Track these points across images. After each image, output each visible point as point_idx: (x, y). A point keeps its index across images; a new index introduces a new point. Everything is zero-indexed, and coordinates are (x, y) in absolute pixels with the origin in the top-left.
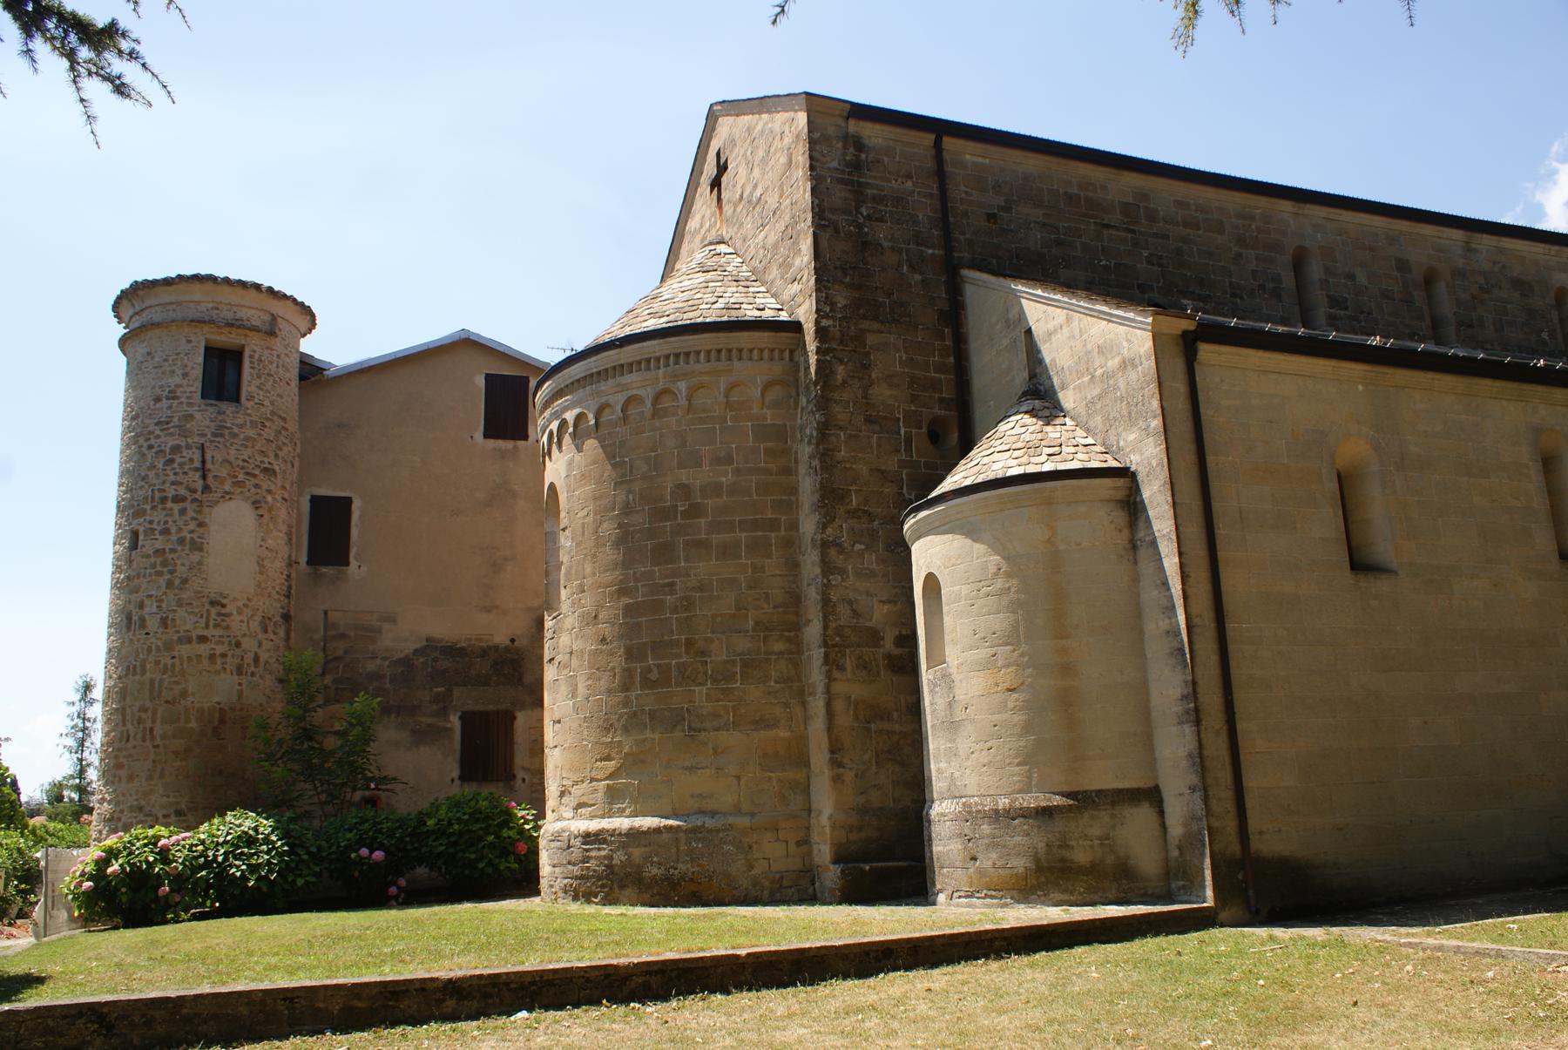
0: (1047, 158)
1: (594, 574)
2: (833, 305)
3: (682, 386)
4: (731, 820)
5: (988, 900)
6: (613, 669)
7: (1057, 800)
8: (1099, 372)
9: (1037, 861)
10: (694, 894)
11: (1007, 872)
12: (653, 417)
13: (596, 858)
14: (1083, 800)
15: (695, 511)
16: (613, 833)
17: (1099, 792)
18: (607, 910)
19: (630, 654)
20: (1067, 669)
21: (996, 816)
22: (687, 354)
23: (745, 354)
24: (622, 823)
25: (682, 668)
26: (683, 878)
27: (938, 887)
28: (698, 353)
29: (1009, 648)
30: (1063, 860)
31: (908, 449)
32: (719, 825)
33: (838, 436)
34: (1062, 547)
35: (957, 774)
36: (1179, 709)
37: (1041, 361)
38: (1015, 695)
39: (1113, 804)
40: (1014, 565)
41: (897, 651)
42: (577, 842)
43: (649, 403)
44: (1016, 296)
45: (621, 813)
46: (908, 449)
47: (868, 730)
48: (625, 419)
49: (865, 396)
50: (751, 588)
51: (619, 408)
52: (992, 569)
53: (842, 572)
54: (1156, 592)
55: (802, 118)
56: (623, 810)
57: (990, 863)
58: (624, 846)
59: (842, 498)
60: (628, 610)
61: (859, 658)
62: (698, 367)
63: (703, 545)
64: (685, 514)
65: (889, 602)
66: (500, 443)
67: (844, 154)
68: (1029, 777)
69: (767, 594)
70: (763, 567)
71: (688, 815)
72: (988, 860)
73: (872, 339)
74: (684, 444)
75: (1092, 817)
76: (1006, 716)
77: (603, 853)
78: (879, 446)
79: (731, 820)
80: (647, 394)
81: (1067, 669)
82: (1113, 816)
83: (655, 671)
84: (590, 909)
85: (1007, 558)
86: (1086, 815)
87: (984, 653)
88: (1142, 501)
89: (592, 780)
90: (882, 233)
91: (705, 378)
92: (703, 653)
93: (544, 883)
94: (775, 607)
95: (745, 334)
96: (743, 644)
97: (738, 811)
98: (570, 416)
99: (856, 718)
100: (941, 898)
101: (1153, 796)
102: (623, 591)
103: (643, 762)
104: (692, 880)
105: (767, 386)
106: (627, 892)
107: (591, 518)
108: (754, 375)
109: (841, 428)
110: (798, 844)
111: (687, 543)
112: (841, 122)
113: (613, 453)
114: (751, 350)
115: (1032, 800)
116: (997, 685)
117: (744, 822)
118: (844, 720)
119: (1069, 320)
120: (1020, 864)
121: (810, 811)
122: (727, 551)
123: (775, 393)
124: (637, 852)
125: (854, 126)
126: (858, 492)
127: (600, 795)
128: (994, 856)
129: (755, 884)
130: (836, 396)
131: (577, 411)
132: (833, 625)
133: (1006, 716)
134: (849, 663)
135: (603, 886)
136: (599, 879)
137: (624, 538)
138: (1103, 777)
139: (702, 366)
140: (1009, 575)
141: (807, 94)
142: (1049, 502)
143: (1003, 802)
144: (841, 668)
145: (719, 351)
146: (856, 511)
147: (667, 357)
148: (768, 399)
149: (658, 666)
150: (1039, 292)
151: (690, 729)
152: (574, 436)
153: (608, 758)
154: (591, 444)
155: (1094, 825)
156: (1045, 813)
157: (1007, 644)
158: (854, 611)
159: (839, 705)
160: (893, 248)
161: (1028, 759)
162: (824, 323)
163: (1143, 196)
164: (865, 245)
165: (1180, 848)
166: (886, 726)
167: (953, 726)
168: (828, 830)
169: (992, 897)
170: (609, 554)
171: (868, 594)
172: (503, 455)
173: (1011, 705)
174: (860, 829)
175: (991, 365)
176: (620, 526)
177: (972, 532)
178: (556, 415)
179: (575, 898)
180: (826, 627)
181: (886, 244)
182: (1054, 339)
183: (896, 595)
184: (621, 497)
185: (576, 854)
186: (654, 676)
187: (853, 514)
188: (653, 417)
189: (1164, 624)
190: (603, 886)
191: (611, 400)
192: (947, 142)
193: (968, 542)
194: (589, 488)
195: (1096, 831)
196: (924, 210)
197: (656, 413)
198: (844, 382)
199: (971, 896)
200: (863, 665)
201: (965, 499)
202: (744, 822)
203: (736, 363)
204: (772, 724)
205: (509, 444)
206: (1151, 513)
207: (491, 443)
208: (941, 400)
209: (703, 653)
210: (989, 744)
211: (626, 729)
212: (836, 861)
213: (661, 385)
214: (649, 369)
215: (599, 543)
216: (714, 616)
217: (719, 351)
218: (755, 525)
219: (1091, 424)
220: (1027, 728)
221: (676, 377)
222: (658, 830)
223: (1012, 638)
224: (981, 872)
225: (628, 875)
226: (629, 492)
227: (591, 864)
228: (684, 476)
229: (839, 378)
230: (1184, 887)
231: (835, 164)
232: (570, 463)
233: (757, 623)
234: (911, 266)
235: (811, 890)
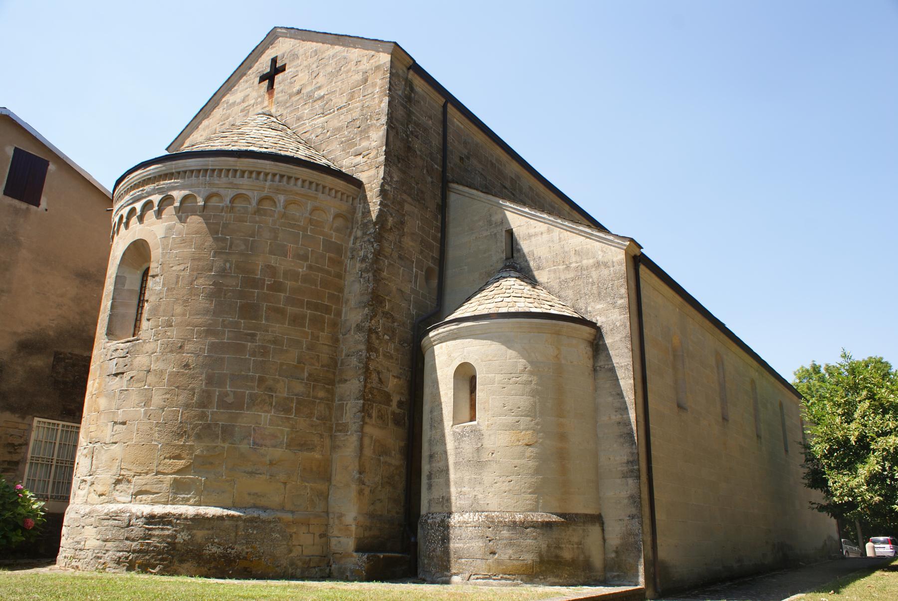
0: (489, 140)
1: (184, 315)
2: (391, 177)
3: (282, 198)
4: (279, 514)
5: (503, 581)
6: (193, 389)
7: (554, 518)
8: (573, 265)
9: (540, 555)
10: (245, 569)
11: (520, 562)
12: (255, 213)
13: (158, 536)
14: (569, 519)
15: (277, 287)
16: (179, 517)
17: (577, 515)
18: (165, 579)
19: (210, 380)
20: (562, 437)
21: (514, 525)
22: (289, 178)
23: (327, 190)
24: (189, 510)
25: (253, 398)
26: (238, 556)
27: (453, 571)
28: (297, 179)
29: (529, 418)
30: (557, 556)
31: (416, 282)
32: (271, 518)
33: (384, 262)
34: (563, 362)
35: (480, 496)
36: (625, 469)
37: (520, 250)
38: (530, 449)
39: (584, 523)
40: (535, 368)
41: (398, 411)
42: (140, 522)
43: (254, 202)
44: (500, 207)
45: (185, 501)
46: (416, 282)
47: (379, 460)
48: (232, 209)
49: (400, 242)
50: (308, 349)
51: (228, 200)
52: (520, 367)
53: (377, 351)
54: (610, 399)
55: (385, 58)
56: (188, 500)
57: (507, 556)
58: (189, 528)
59: (381, 303)
60: (213, 347)
61: (379, 411)
62: (295, 188)
63: (281, 312)
64: (270, 287)
65: (397, 377)
66: (16, 203)
67: (405, 89)
68: (537, 502)
69: (318, 356)
70: (318, 337)
71: (245, 508)
72: (505, 554)
73: (407, 207)
74: (276, 238)
75: (574, 530)
76: (524, 461)
77: (166, 533)
78: (403, 275)
79: (279, 514)
80: (254, 196)
81: (562, 437)
82: (584, 530)
83: (232, 395)
84: (193, 579)
85: (531, 362)
86: (571, 529)
87: (510, 419)
88: (605, 345)
89: (158, 473)
90: (417, 145)
91: (298, 198)
92: (271, 389)
93: (60, 557)
94: (322, 366)
95: (330, 178)
96: (299, 388)
97: (283, 509)
98: (178, 195)
99: (374, 452)
100: (455, 579)
101: (597, 519)
102: (210, 331)
103: (211, 463)
104: (245, 558)
105: (337, 216)
106: (186, 565)
107: (188, 272)
108: (331, 206)
109: (386, 257)
110: (321, 536)
111: (268, 308)
112: (405, 70)
113: (216, 229)
114: (331, 189)
115: (539, 517)
116: (519, 441)
117: (289, 517)
118: (368, 452)
119: (549, 231)
120: (529, 558)
121: (327, 513)
122: (297, 320)
123: (339, 222)
124: (200, 534)
125: (411, 75)
126: (390, 301)
127: (165, 486)
128: (511, 551)
129: (292, 564)
130: (386, 235)
131: (186, 192)
132: (369, 385)
133: (524, 461)
134: (374, 414)
135: (162, 560)
136: (159, 553)
137: (217, 293)
138: (580, 506)
139: (298, 188)
140: (531, 373)
141: (395, 43)
142: (558, 333)
143: (519, 517)
144: (370, 416)
145: (311, 183)
146: (387, 313)
147: (274, 175)
148: (335, 226)
149: (235, 392)
150: (527, 210)
151: (254, 443)
152: (178, 210)
153: (178, 457)
154: (195, 221)
155: (573, 535)
156: (548, 525)
157: (527, 416)
158: (380, 379)
159: (367, 441)
160: (421, 156)
161: (537, 490)
162: (387, 187)
163: (518, 177)
164: (409, 148)
165: (616, 552)
166: (388, 459)
167: (478, 464)
168: (353, 528)
169: (506, 579)
170: (201, 302)
171: (388, 370)
172: (17, 211)
173: (527, 454)
174: (370, 529)
175: (465, 243)
176: (214, 284)
177: (507, 342)
178: (160, 191)
179: (130, 568)
180: (365, 386)
181: (418, 153)
182: (533, 239)
183: (401, 374)
184: (219, 263)
185: (137, 531)
186: (230, 399)
187: (386, 314)
188: (255, 213)
189: (616, 417)
190: (162, 560)
191: (222, 192)
192: (450, 108)
193: (504, 347)
194: (189, 251)
195: (575, 539)
196: (436, 141)
197: (258, 212)
198: (391, 228)
199: (490, 578)
200: (381, 417)
201: (506, 320)
202: (289, 517)
203: (320, 195)
204: (312, 449)
205: (24, 206)
206: (612, 353)
207: (9, 200)
208: (433, 257)
209: (271, 389)
210: (510, 478)
211: (199, 437)
212: (358, 550)
213: (265, 193)
214: (257, 179)
215: (193, 292)
216: (282, 364)
217: (311, 183)
218: (316, 307)
219: (563, 294)
220: (537, 471)
221: (278, 191)
222: (221, 518)
223: (531, 413)
224: (499, 563)
225: (187, 552)
226: (226, 261)
227: (154, 541)
228: (273, 260)
229: (389, 224)
230: (618, 576)
231: (400, 93)
232: (170, 229)
233: (310, 375)
234: (427, 171)
235: (327, 571)
